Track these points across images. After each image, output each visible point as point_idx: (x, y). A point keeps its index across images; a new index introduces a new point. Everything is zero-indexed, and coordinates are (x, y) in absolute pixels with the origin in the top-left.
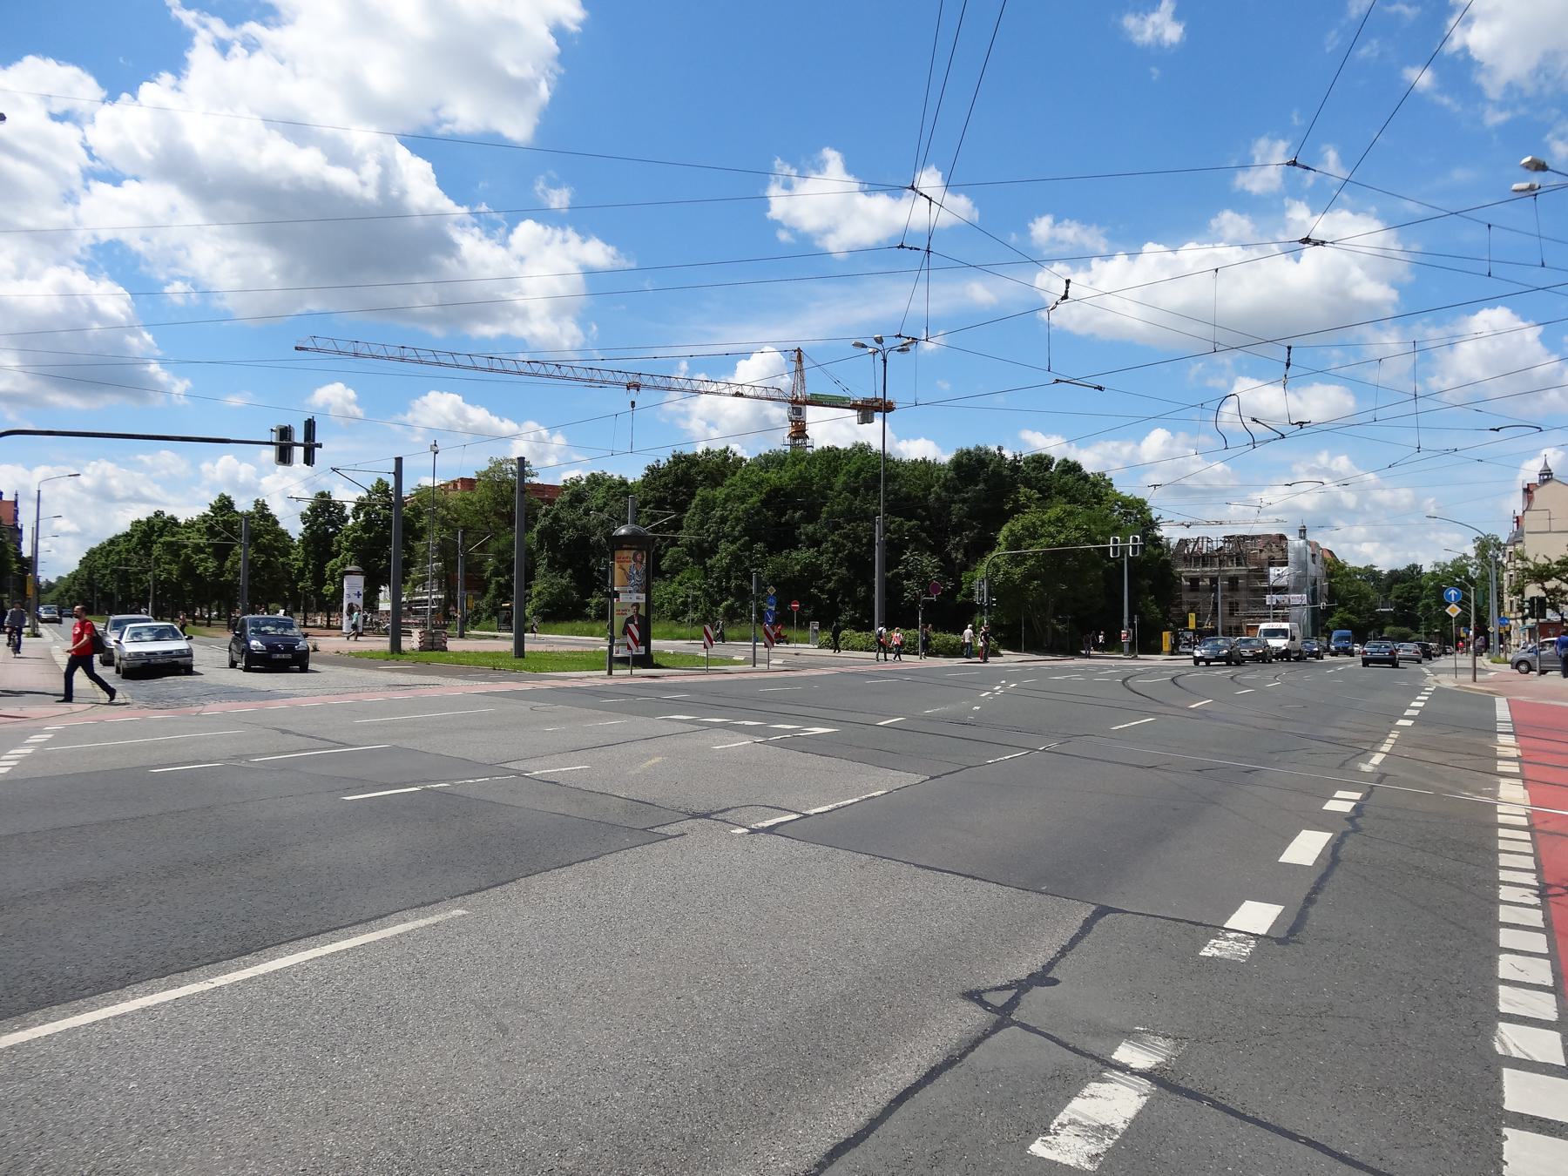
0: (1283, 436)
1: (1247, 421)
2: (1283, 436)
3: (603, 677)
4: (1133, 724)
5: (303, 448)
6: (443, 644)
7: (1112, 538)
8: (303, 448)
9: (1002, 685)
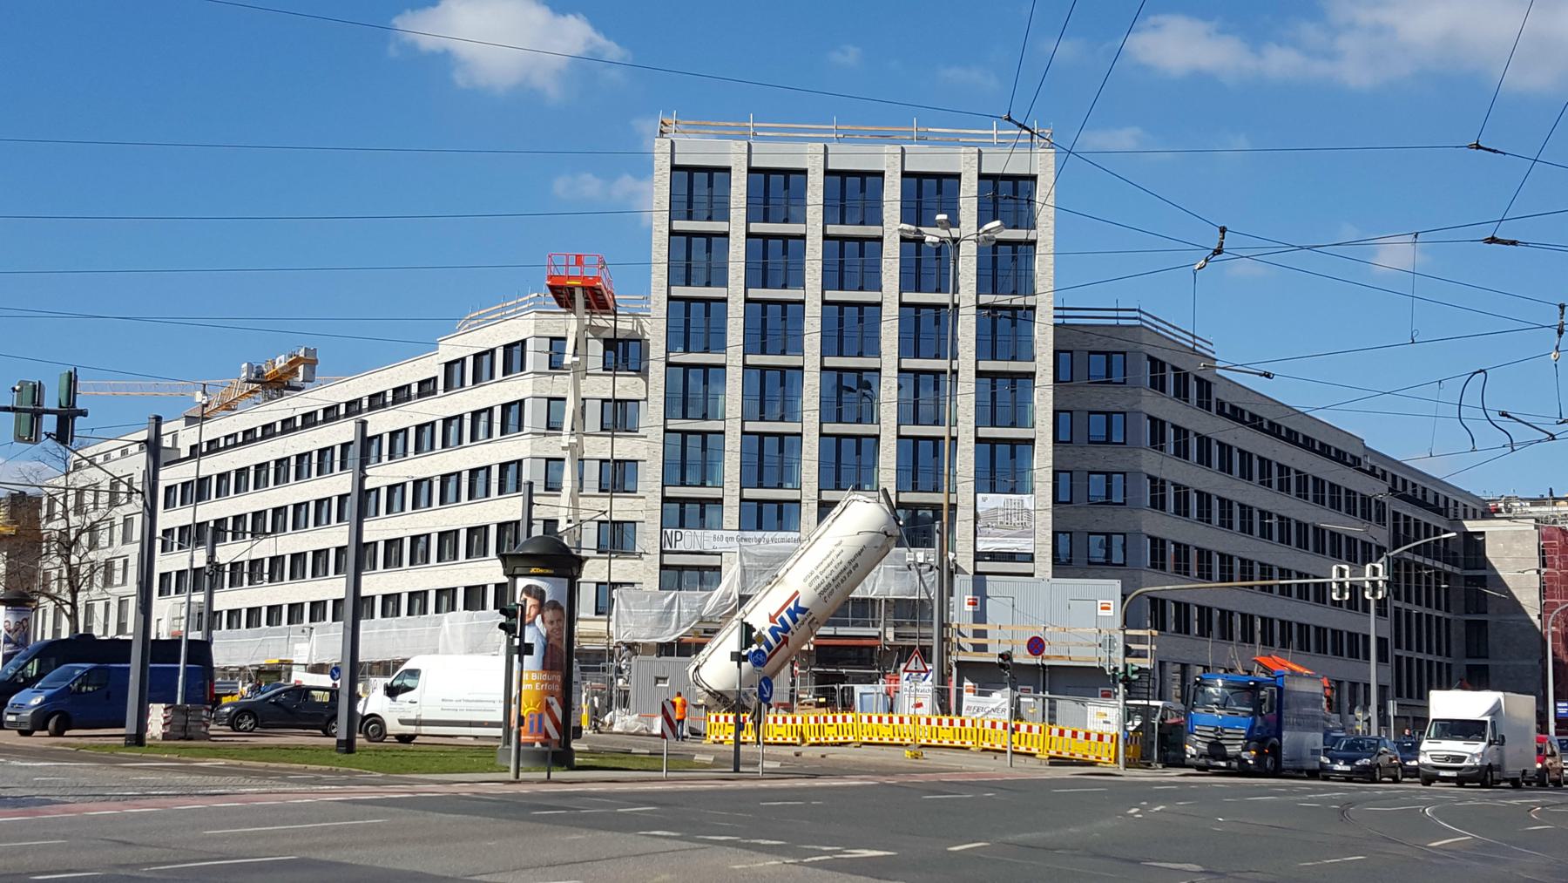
0: (1553, 437)
1: (1494, 416)
2: (1553, 437)
4: (768, 842)
5: (56, 416)
6: (203, 729)
7: (1335, 568)
8: (56, 416)
9: (1142, 808)
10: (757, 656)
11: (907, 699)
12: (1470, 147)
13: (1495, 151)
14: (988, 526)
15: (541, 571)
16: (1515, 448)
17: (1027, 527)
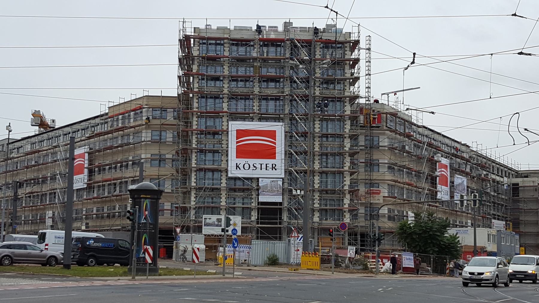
1: (522, 130)
3: (129, 280)
11: (293, 248)
12: (513, 15)
13: (522, 17)
14: (264, 191)
15: (145, 196)
16: (530, 144)
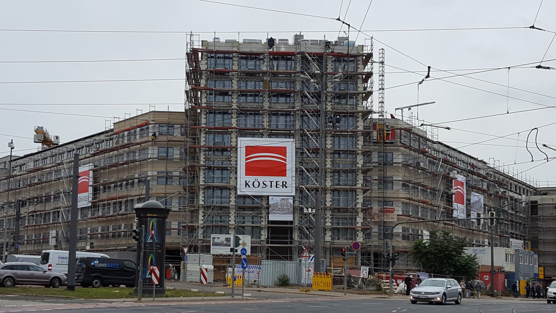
1: (541, 146)
3: (135, 302)
10: (243, 251)
12: (531, 27)
13: (540, 29)
14: (274, 210)
16: (549, 160)
17: (290, 210)
